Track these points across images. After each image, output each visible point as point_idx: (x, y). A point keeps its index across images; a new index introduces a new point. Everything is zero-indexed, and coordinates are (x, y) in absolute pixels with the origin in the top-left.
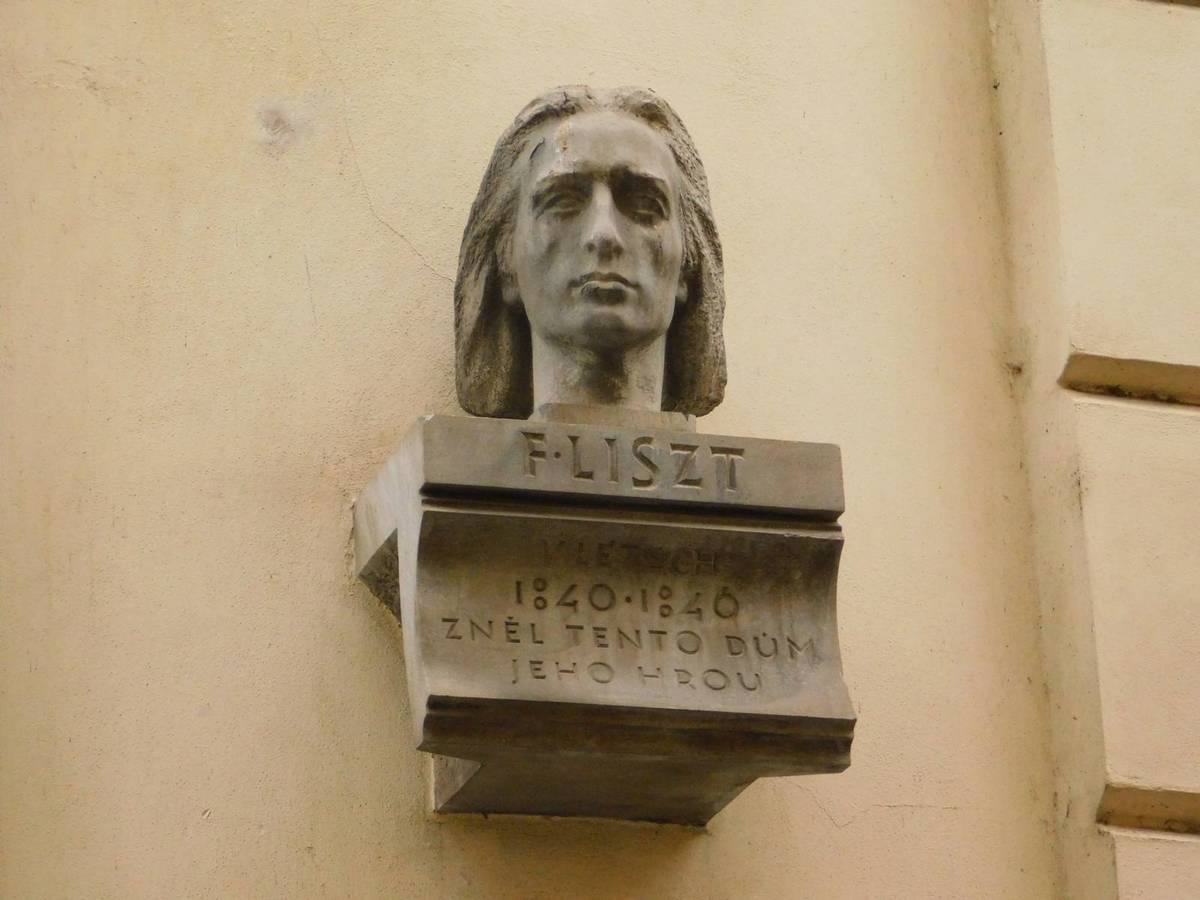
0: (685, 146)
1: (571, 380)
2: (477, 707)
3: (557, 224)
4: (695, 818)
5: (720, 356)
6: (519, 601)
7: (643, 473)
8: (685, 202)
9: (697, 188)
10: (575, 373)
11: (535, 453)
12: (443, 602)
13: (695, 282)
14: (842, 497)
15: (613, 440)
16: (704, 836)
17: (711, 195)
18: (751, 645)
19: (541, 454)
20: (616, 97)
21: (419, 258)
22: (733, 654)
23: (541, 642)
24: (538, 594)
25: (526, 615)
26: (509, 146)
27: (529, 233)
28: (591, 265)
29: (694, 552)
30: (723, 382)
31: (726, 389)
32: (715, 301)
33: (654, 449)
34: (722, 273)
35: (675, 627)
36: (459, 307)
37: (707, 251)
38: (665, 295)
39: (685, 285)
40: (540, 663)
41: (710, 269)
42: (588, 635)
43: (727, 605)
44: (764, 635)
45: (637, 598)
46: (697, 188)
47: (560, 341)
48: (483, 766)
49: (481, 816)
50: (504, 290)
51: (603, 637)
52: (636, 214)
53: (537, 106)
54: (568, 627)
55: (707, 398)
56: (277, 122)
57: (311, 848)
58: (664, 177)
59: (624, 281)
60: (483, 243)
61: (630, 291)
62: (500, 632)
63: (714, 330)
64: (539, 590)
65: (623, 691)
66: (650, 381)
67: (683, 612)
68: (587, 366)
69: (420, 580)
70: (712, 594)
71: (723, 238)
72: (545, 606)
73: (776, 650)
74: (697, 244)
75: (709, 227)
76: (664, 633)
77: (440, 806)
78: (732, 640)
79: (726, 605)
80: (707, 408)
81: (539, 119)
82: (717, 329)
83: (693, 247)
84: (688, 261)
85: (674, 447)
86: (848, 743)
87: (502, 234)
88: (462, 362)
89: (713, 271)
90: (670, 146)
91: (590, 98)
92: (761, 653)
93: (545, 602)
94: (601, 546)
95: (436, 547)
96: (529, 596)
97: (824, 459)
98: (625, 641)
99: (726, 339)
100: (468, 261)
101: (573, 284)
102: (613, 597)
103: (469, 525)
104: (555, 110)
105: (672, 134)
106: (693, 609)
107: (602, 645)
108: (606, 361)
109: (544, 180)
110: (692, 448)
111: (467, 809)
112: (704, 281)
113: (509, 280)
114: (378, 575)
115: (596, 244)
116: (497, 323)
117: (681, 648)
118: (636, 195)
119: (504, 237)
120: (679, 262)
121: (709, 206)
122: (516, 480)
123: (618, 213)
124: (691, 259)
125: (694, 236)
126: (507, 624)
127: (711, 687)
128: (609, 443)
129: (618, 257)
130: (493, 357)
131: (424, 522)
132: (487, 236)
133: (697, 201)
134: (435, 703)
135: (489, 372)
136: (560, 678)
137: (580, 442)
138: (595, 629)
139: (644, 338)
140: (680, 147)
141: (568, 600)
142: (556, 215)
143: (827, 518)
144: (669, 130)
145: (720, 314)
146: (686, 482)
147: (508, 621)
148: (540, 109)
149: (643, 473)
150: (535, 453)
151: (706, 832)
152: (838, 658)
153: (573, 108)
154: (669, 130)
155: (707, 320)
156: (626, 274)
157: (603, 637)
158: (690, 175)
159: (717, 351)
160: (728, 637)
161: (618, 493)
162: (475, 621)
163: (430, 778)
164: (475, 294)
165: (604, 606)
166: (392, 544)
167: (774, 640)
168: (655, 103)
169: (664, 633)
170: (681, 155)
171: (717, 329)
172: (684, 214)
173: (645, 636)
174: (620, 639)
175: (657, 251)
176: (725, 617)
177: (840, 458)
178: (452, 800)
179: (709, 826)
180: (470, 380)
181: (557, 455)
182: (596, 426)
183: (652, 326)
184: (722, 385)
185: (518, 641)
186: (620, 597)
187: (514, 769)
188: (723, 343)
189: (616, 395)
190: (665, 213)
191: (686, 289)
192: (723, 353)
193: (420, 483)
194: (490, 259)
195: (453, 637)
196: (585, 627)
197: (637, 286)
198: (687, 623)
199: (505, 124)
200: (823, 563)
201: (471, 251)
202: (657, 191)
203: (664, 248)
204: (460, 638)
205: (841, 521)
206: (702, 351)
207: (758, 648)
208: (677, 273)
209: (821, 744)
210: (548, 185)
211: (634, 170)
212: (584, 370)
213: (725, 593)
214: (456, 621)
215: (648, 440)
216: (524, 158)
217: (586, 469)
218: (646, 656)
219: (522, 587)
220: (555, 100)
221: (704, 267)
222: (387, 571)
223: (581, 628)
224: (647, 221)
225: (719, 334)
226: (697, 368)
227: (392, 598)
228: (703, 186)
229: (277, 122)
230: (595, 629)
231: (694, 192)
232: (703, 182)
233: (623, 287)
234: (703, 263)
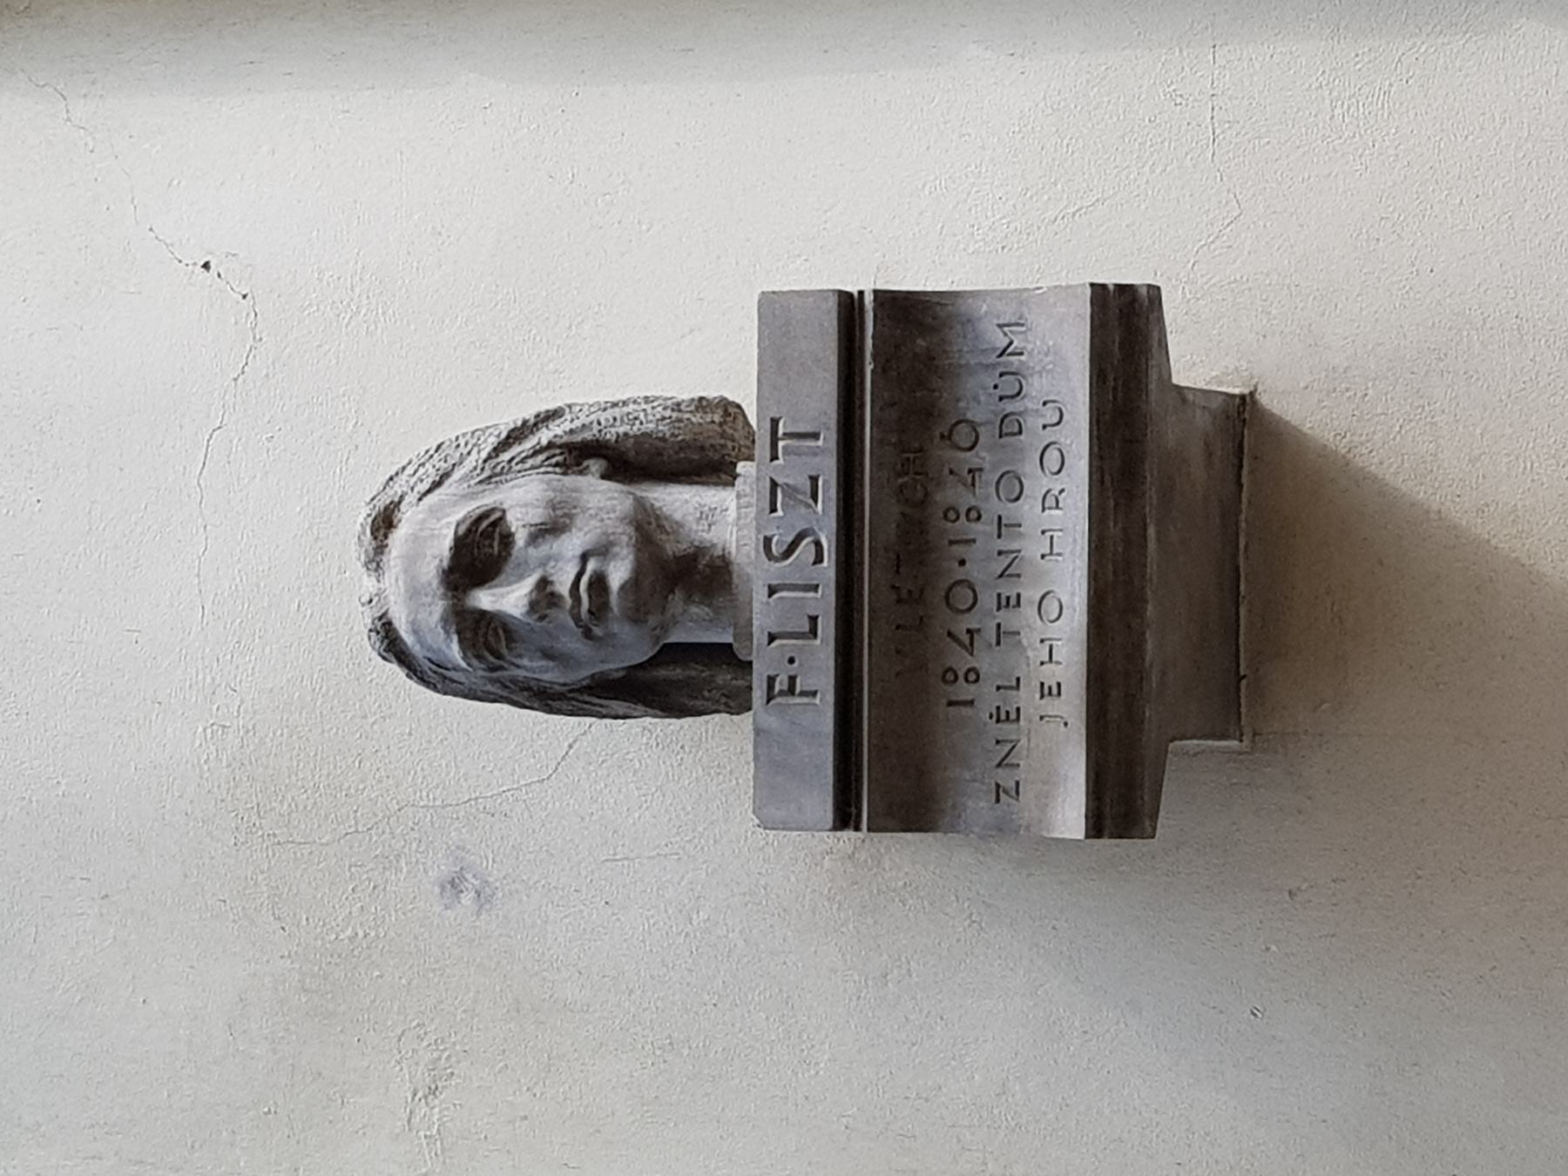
2: (1097, 775)
11: (791, 691)
13: (577, 454)
15: (770, 587)
16: (1257, 396)
18: (1009, 407)
19: (792, 679)
22: (1020, 432)
23: (1018, 680)
24: (963, 517)
29: (900, 481)
35: (994, 506)
37: (544, 436)
38: (602, 500)
39: (586, 463)
44: (996, 387)
45: (958, 550)
49: (1244, 682)
51: (1008, 598)
54: (998, 643)
57: (1290, 892)
68: (689, 599)
74: (535, 453)
76: (1000, 518)
79: (963, 436)
83: (541, 457)
84: (557, 465)
85: (773, 510)
86: (1121, 288)
92: (1019, 393)
93: (969, 670)
94: (899, 601)
96: (964, 691)
101: (588, 634)
106: (967, 642)
107: (1018, 604)
117: (1017, 499)
122: (822, 715)
123: (503, 576)
124: (554, 461)
126: (998, 721)
129: (551, 583)
133: (484, 455)
137: (774, 630)
138: (999, 609)
141: (966, 639)
143: (849, 305)
146: (815, 497)
149: (805, 549)
156: (571, 571)
157: (1008, 598)
165: (971, 594)
167: (1001, 375)
168: (370, 520)
169: (1000, 518)
172: (501, 474)
173: (1002, 544)
174: (1010, 575)
185: (1018, 709)
186: (960, 574)
189: (718, 563)
190: (498, 515)
197: (584, 558)
200: (904, 310)
203: (538, 521)
204: (1017, 783)
205: (854, 290)
208: (571, 480)
209: (1125, 323)
211: (445, 564)
213: (947, 437)
214: (998, 786)
215: (768, 541)
218: (1033, 548)
219: (954, 698)
223: (999, 625)
224: (507, 539)
226: (683, 446)
230: (999, 609)
231: (470, 462)
234: (558, 441)
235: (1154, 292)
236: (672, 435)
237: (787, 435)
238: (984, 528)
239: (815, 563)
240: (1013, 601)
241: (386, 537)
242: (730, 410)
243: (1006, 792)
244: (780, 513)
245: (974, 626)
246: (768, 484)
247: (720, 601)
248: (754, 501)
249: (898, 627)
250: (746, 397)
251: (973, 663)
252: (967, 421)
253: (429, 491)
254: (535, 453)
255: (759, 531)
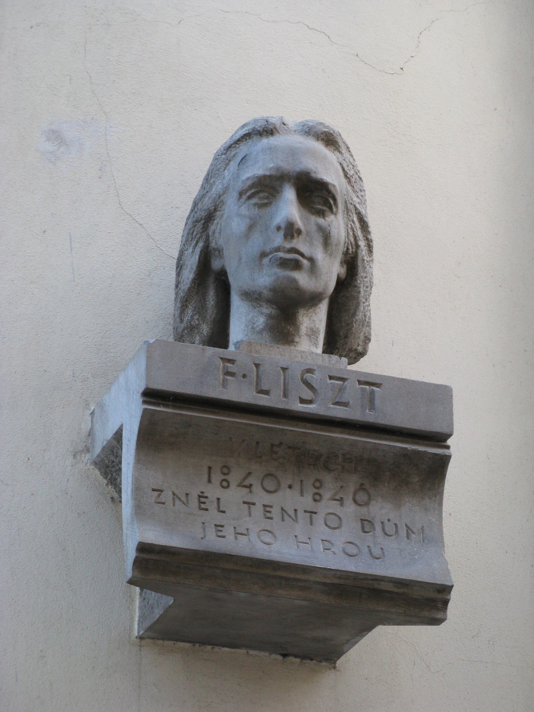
0: (351, 166)
1: (257, 326)
3: (256, 211)
4: (327, 655)
5: (367, 320)
6: (209, 481)
7: (307, 394)
8: (349, 205)
9: (358, 197)
10: (261, 321)
11: (228, 373)
12: (154, 477)
13: (352, 264)
14: (452, 424)
15: (287, 369)
17: (368, 203)
19: (232, 374)
20: (303, 126)
21: (152, 240)
22: (365, 532)
23: (224, 512)
24: (223, 477)
25: (213, 492)
26: (223, 156)
27: (234, 218)
28: (278, 240)
29: (340, 455)
30: (367, 339)
31: (370, 344)
32: (366, 280)
33: (315, 378)
34: (372, 261)
35: (327, 506)
36: (179, 272)
37: (362, 243)
38: (331, 270)
39: (345, 267)
40: (222, 526)
41: (363, 256)
42: (258, 510)
43: (364, 494)
44: (389, 520)
45: (297, 486)
46: (358, 197)
47: (252, 297)
48: (174, 600)
50: (213, 261)
51: (270, 512)
52: (312, 208)
53: (246, 128)
55: (356, 350)
56: (56, 136)
58: (336, 183)
59: (302, 255)
60: (200, 225)
61: (305, 262)
62: (194, 502)
63: (364, 300)
64: (224, 474)
65: (285, 546)
66: (315, 332)
67: (329, 500)
68: (270, 317)
69: (138, 460)
70: (352, 489)
71: (374, 235)
72: (228, 486)
73: (397, 531)
74: (355, 237)
75: (364, 225)
76: (315, 513)
77: (141, 633)
78: (365, 522)
79: (362, 497)
80: (355, 358)
81: (247, 136)
82: (366, 299)
83: (352, 240)
84: (348, 249)
85: (331, 378)
86: (446, 602)
87: (214, 220)
88: (177, 313)
89: (365, 258)
90: (341, 164)
91: (284, 124)
92: (386, 534)
93: (228, 482)
94: (272, 445)
95: (151, 437)
96: (217, 477)
97: (440, 396)
98: (286, 517)
99: (372, 307)
100: (190, 237)
102: (279, 484)
103: (175, 421)
104: (259, 131)
105: (342, 156)
106: (337, 497)
108: (284, 309)
109: (248, 179)
110: (343, 379)
111: (162, 633)
112: (359, 264)
113: (217, 253)
114: (107, 461)
115: (283, 226)
116: (207, 285)
117: (326, 525)
118: (314, 193)
119: (215, 222)
120: (342, 249)
121: (365, 211)
123: (302, 209)
124: (350, 247)
125: (353, 231)
127: (347, 554)
128: (283, 371)
129: (298, 236)
130: (201, 309)
131: (143, 417)
132: (204, 221)
133: (357, 205)
134: (143, 548)
135: (198, 319)
136: (236, 538)
137: (261, 368)
139: (313, 300)
140: (348, 166)
141: (246, 483)
142: (255, 204)
143: (440, 439)
144: (340, 152)
145: (369, 289)
147: (201, 494)
148: (249, 130)
149: (307, 394)
150: (228, 373)
151: (335, 668)
152: (443, 542)
153: (272, 130)
154: (340, 152)
155: (359, 292)
157: (270, 512)
158: (353, 187)
159: (365, 316)
160: (362, 520)
161: (287, 407)
162: (175, 492)
163: (133, 610)
164: (192, 261)
166: (118, 436)
167: (395, 524)
168: (332, 132)
169: (315, 513)
170: (348, 171)
171: (366, 299)
173: (300, 514)
174: (282, 515)
175: (327, 235)
176: (360, 505)
177: (452, 396)
178: (150, 628)
179: (339, 663)
180: (183, 325)
181: (244, 376)
182: (276, 355)
183: (320, 290)
184: (367, 341)
185: (207, 510)
186: (285, 483)
187: (199, 602)
188: (370, 311)
190: (334, 210)
191: (345, 269)
192: (370, 318)
193: (142, 389)
194: (204, 237)
195: (159, 503)
196: (257, 504)
197: (311, 260)
198: (334, 507)
199: (224, 138)
200: (436, 470)
201: (192, 231)
202: (329, 192)
204: (164, 503)
205: (449, 442)
206: (354, 314)
207: (383, 530)
209: (425, 603)
210: (249, 183)
211: (313, 175)
212: (267, 320)
213: (362, 488)
214: (161, 491)
215: (310, 371)
216: (233, 166)
217: (265, 388)
219: (213, 471)
220: (259, 124)
221: (359, 254)
222: (113, 458)
223: (254, 504)
224: (321, 214)
225: (367, 304)
226: (349, 325)
227: (116, 479)
228: (362, 196)
229: (56, 136)
231: (355, 199)
232: (363, 194)
233: (300, 258)
234: (359, 251)
235: (437, 622)
236: (357, 320)
237: (372, 392)
238: (307, 501)
239: (300, 398)
240: (268, 515)
241: (322, 140)
242: (356, 356)
243: (159, 495)
244: (329, 381)
245: (254, 488)
246: (345, 376)
247: (266, 336)
248: (327, 364)
249: (258, 443)
250: (364, 366)
251: (233, 486)
252: (370, 499)
253: (343, 170)
254: (355, 237)
255: (319, 366)
